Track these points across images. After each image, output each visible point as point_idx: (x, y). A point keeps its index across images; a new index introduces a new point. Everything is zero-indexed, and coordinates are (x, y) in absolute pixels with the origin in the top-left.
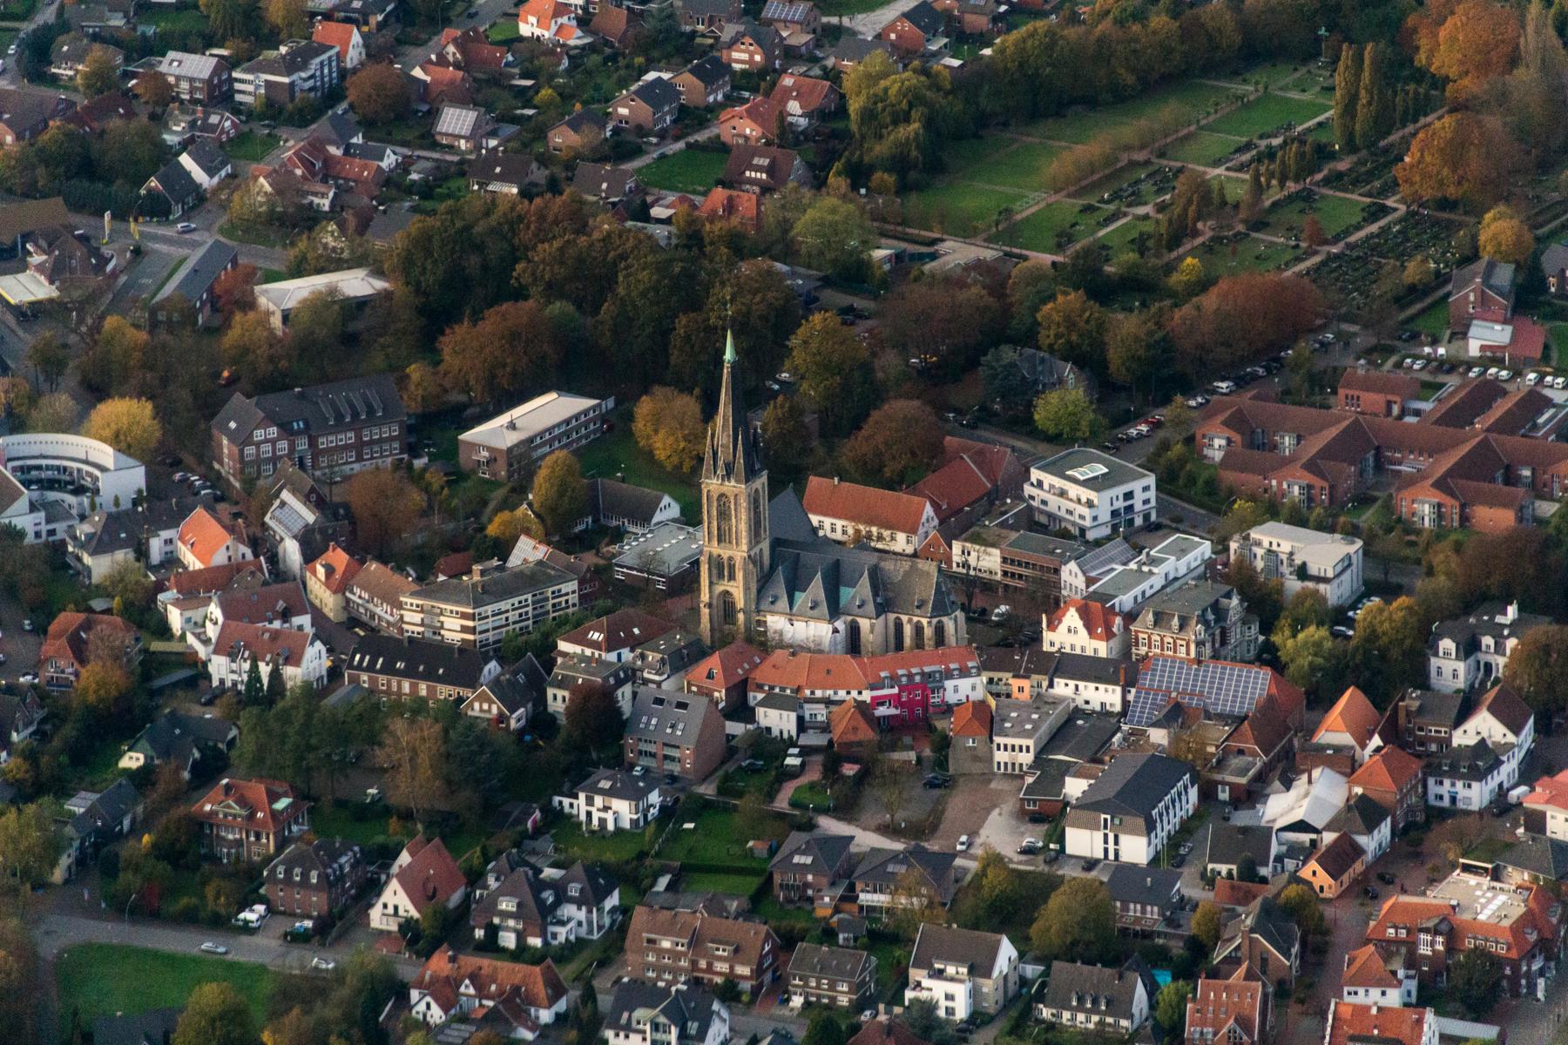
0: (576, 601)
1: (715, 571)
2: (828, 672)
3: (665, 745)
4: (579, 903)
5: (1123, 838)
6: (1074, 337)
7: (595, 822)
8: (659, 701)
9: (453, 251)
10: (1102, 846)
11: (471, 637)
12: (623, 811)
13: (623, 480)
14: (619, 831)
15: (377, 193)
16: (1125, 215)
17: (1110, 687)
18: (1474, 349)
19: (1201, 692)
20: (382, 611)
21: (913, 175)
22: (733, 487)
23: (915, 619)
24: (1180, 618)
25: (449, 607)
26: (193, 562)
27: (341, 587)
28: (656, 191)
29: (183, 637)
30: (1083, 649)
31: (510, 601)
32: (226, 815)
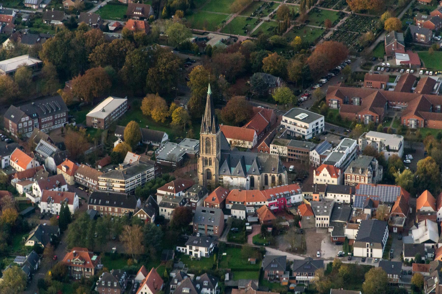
0: (154, 174)
1: (204, 163)
2: (253, 196)
3: (208, 226)
4: (208, 287)
5: (374, 250)
6: (276, 68)
7: (193, 255)
8: (204, 211)
9: (65, 50)
10: (366, 253)
11: (124, 189)
12: (203, 251)
13: (148, 128)
14: (202, 257)
15: (15, 26)
16: (262, 20)
17: (347, 195)
18: (398, 62)
19: (378, 196)
20: (90, 181)
21: (188, 10)
22: (211, 135)
23: (272, 174)
24: (362, 169)
25: (116, 180)
26: (19, 169)
27: (73, 174)
28: (107, 20)
29: (24, 195)
30: (329, 181)
31: (135, 176)
32: (76, 263)
